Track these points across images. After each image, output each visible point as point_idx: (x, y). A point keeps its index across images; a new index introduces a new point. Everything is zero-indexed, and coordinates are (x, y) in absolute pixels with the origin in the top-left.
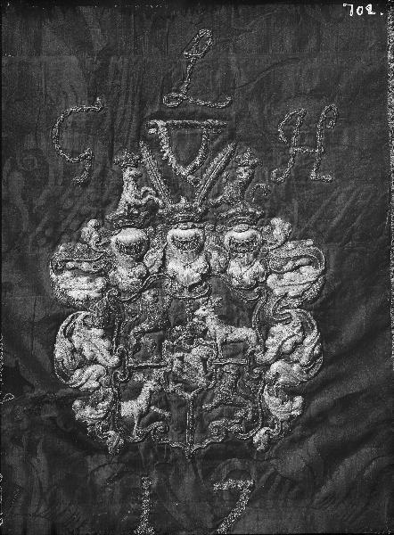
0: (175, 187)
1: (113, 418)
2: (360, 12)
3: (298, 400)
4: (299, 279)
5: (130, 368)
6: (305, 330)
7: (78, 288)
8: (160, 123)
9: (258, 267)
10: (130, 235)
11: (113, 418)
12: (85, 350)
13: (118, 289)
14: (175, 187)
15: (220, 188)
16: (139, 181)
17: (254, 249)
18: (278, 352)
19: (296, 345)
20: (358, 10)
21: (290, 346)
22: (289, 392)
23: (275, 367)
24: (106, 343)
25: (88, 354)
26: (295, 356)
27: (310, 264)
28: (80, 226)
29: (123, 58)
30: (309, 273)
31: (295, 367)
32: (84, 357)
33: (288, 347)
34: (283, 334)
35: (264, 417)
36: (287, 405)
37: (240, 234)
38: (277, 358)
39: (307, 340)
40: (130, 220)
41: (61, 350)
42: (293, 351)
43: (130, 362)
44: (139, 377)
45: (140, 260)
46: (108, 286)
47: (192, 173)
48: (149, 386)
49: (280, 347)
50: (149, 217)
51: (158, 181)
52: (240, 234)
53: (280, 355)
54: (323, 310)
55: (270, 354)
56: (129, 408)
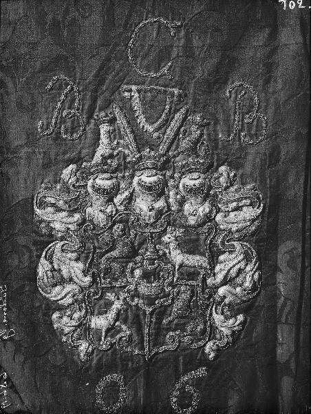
0: (141, 141)
1: (84, 328)
2: (292, 4)
3: (240, 318)
4: (241, 216)
5: (103, 288)
6: (247, 258)
7: (60, 222)
8: (134, 88)
9: (206, 207)
10: (103, 182)
11: (84, 328)
12: (63, 273)
13: (94, 224)
14: (141, 141)
15: (178, 145)
16: (114, 134)
17: (205, 193)
18: (225, 277)
19: (240, 271)
20: (294, 5)
21: (234, 270)
22: (233, 310)
23: (222, 291)
24: (81, 265)
25: (65, 273)
26: (239, 280)
27: (251, 205)
28: (63, 168)
29: (42, 204)
30: (249, 213)
31: (238, 289)
32: (62, 276)
33: (233, 272)
34: (229, 262)
35: (212, 332)
36: (231, 321)
37: (189, 181)
38: (224, 283)
39: (248, 268)
40: (104, 166)
41: (43, 268)
42: (238, 275)
43: (105, 283)
44: (110, 296)
45: (110, 200)
46: (84, 221)
47: (157, 130)
48: (117, 305)
49: (281, 270)
50: (121, 167)
51: (130, 138)
52: (189, 181)
53: (224, 283)
54: (263, 241)
55: (220, 277)
56: (100, 322)
